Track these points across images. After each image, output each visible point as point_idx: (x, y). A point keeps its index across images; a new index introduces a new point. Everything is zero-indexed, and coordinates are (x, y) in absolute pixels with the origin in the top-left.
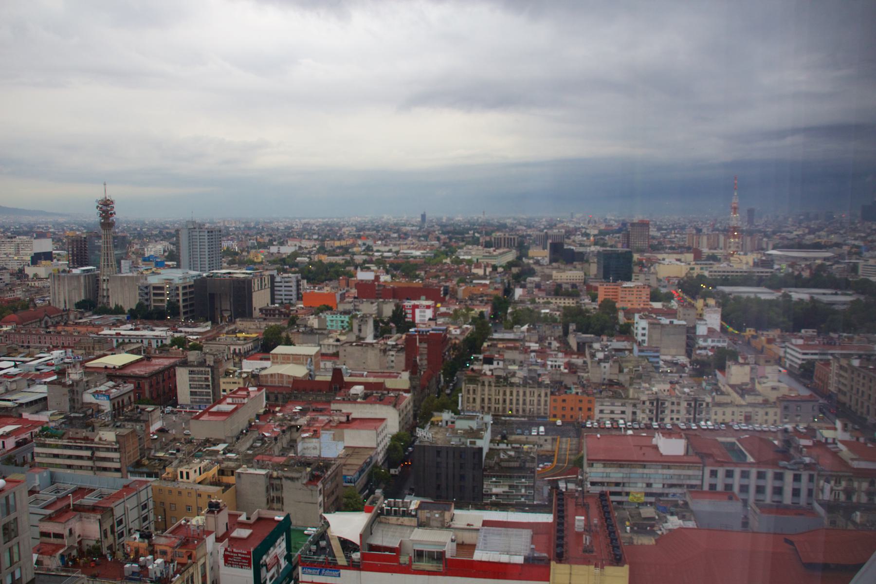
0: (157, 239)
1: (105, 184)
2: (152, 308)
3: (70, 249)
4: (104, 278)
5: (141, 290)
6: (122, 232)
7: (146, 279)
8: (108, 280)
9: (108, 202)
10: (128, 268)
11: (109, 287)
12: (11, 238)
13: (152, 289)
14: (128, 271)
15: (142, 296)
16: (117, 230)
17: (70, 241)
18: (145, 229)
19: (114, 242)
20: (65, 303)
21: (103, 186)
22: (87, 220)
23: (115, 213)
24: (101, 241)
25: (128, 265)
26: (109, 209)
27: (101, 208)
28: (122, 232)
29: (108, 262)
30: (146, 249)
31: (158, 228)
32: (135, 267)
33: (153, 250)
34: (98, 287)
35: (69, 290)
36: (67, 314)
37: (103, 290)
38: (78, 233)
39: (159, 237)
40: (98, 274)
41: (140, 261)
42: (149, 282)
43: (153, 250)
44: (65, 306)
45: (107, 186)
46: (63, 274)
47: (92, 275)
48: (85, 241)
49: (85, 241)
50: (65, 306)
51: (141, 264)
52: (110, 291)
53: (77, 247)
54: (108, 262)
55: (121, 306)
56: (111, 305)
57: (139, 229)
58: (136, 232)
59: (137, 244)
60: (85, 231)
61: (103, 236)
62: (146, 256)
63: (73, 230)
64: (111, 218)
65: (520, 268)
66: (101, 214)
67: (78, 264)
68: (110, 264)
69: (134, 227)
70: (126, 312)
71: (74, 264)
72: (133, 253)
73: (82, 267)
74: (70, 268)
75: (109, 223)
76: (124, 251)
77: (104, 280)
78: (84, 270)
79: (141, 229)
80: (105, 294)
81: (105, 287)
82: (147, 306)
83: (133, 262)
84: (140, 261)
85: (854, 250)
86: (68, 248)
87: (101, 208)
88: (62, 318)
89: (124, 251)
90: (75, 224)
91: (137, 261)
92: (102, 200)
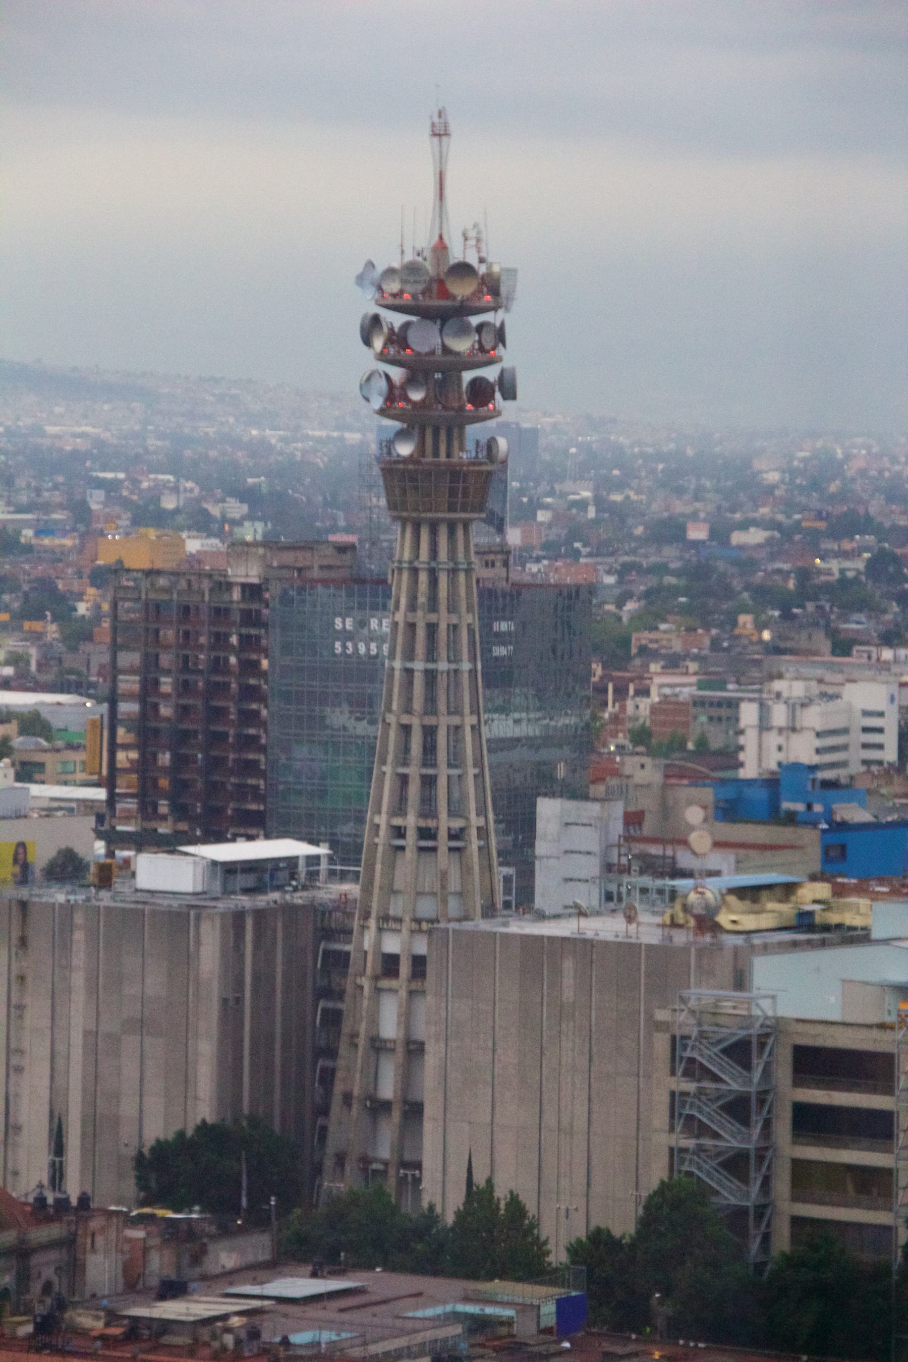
0: (857, 623)
1: (440, 133)
2: (782, 1241)
3: (129, 683)
4: (392, 945)
5: (693, 1069)
6: (553, 551)
7: (740, 981)
8: (419, 963)
9: (461, 290)
10: (591, 867)
11: (421, 1031)
12: (554, 652)
13: (783, 1073)
14: (589, 897)
15: (694, 1127)
16: (514, 537)
17: (130, 611)
18: (755, 536)
19: (491, 638)
20: (58, 1147)
21: (425, 143)
22: (273, 436)
23: (510, 393)
24: (379, 624)
25: (589, 839)
26: (462, 345)
27: (398, 339)
28: (553, 551)
29: (428, 809)
30: (748, 714)
31: (864, 524)
32: (650, 866)
33: (813, 718)
34: (334, 1019)
35: (91, 1036)
36: (69, 1243)
37: (378, 1046)
38: (193, 545)
39: (864, 605)
40: (343, 904)
41: (694, 815)
42: (765, 1008)
43: (813, 718)
44: (57, 1175)
45: (456, 145)
46: (59, 896)
47: (289, 910)
48: (250, 618)
49: (250, 618)
50: (57, 1175)
51: (700, 840)
52: (431, 1061)
53: (185, 665)
54: (428, 809)
55: (516, 1206)
56: (430, 1192)
57: (697, 533)
58: (671, 555)
59: (673, 663)
60: (251, 532)
61: (401, 586)
62: (749, 771)
63: (160, 518)
64: (474, 432)
65: (792, 575)
66: (393, 394)
67: (180, 811)
68: (444, 823)
69: (657, 509)
70: (558, 1256)
71: (148, 810)
72: (641, 737)
73: (218, 837)
74: (113, 839)
75: (456, 474)
76: (567, 720)
77: (390, 964)
78: (230, 869)
79: (721, 534)
80: (387, 1090)
81: (390, 1029)
82: (740, 1213)
83: (633, 819)
84: (694, 815)
85: (44, 813)
86: (113, 671)
87: (398, 339)
88: (24, 1278)
89: (567, 720)
90: (175, 465)
91: (667, 811)
92: (412, 269)
